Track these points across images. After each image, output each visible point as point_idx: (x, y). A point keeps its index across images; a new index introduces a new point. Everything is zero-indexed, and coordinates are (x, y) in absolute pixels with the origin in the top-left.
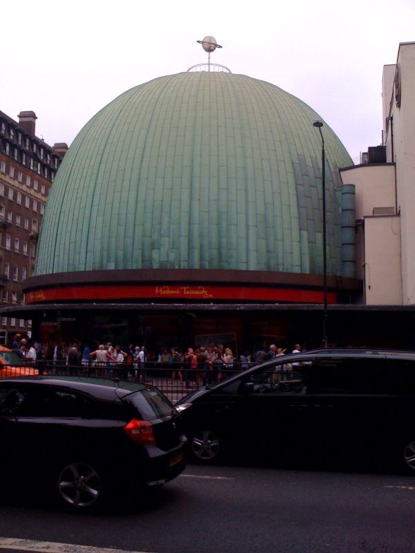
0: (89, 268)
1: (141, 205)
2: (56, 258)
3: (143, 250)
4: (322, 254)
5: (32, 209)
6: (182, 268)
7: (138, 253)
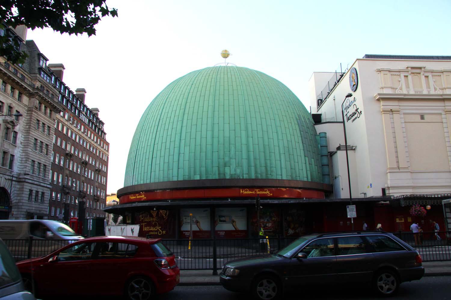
0: (181, 179)
1: (216, 140)
2: (152, 173)
3: (219, 167)
6: (245, 178)
7: (216, 169)
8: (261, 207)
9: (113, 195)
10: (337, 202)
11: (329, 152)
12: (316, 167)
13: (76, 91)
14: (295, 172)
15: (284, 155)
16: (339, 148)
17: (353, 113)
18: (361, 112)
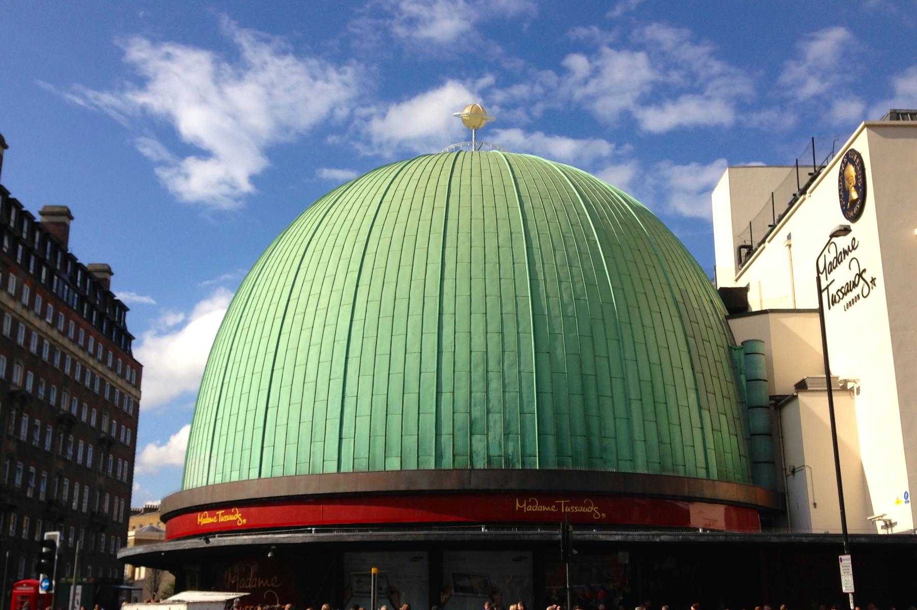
4: (336, 457)
5: (64, 371)
8: (575, 552)
9: (149, 510)
10: (801, 544)
11: (772, 398)
12: (734, 439)
13: (42, 214)
14: (673, 455)
15: (639, 402)
16: (802, 386)
17: (847, 284)
18: (873, 280)
